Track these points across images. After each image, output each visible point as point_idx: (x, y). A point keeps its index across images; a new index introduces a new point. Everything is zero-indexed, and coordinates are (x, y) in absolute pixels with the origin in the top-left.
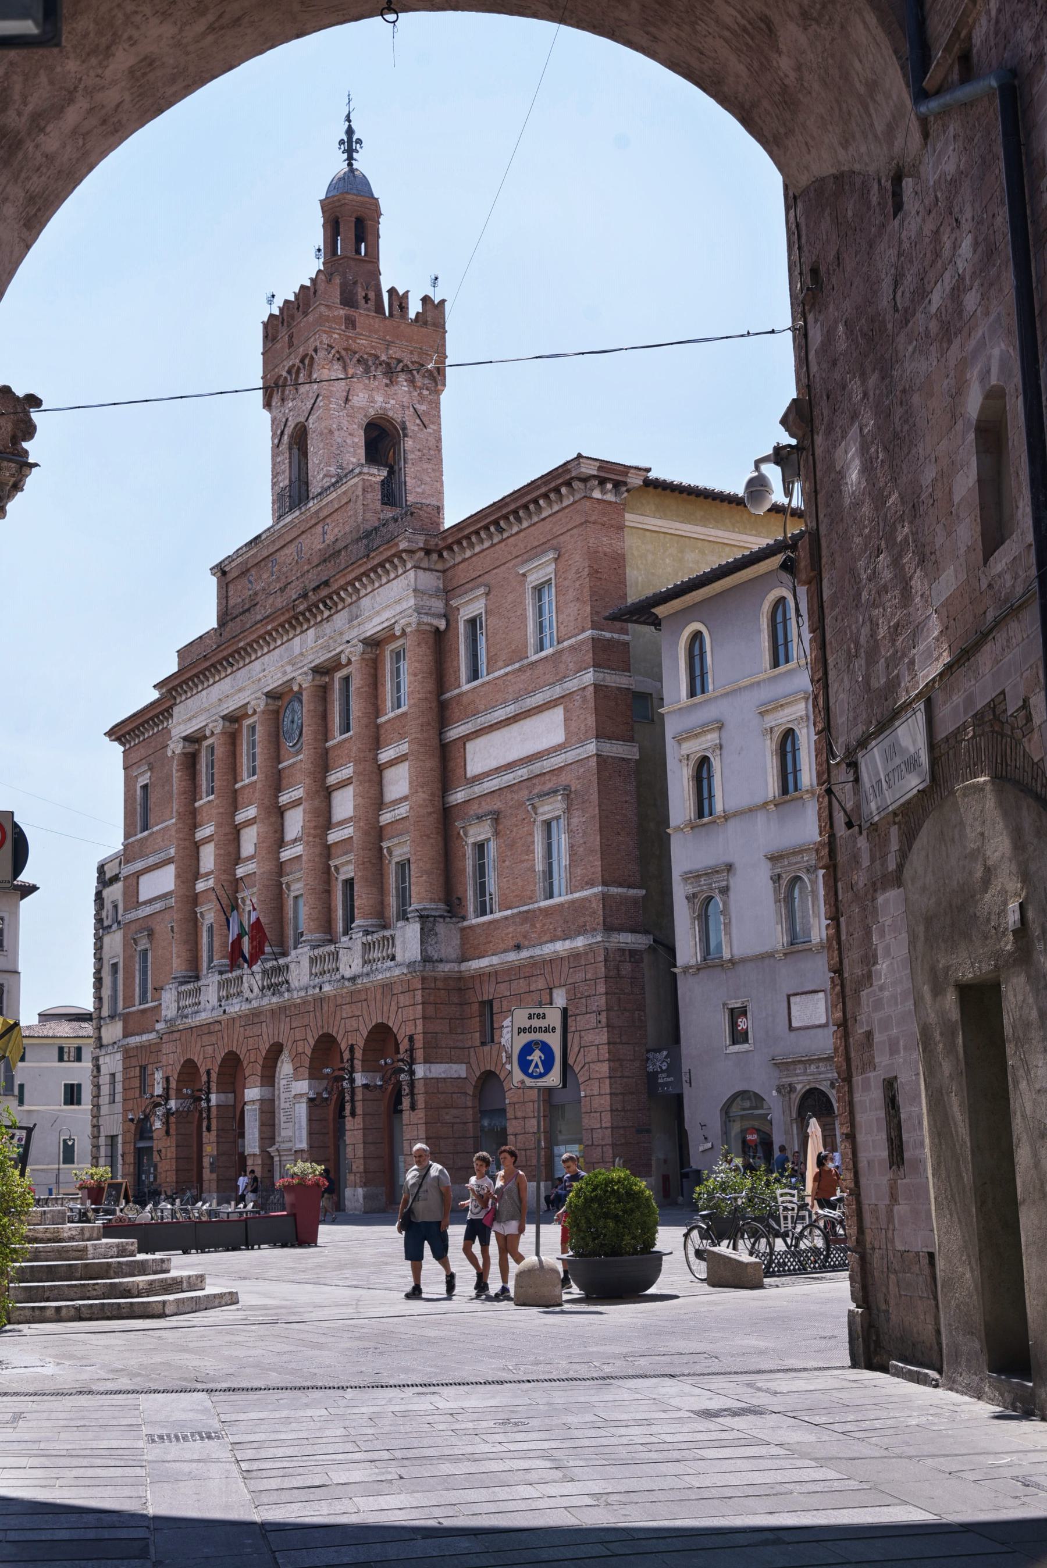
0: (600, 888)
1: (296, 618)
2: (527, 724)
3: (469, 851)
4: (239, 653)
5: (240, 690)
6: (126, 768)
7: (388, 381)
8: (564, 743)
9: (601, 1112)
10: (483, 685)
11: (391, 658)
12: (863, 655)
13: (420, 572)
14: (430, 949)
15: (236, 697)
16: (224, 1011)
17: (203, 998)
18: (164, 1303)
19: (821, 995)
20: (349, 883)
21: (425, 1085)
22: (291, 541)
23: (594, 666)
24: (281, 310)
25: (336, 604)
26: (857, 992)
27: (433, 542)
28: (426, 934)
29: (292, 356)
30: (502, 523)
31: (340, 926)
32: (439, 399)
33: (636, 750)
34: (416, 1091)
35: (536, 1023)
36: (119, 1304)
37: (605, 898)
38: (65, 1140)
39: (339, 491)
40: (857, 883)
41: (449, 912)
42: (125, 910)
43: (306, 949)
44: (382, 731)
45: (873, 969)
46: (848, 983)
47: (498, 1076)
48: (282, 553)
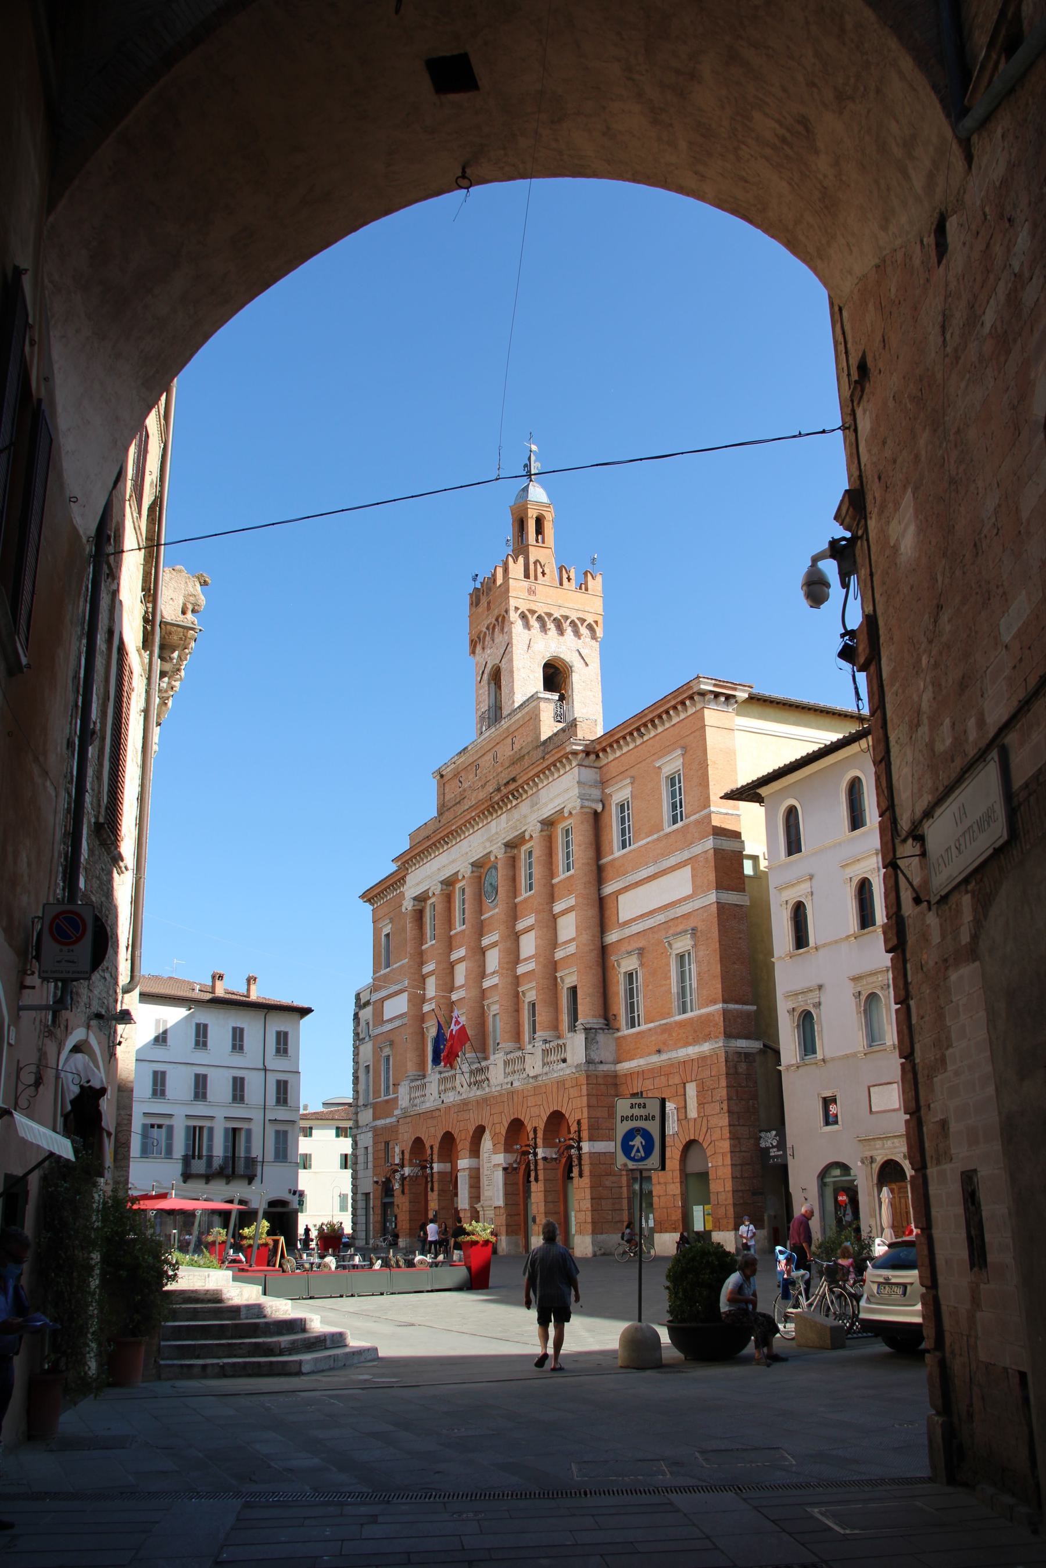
1: (491, 808)
5: (453, 861)
10: (630, 852)
12: (926, 721)
14: (592, 1053)
17: (427, 1092)
18: (300, 1362)
19: (895, 1085)
21: (590, 1157)
25: (521, 795)
26: (930, 1077)
28: (589, 1042)
30: (642, 730)
33: (747, 898)
35: (637, 1112)
36: (259, 1363)
37: (725, 1012)
40: (927, 963)
42: (374, 1026)
44: (556, 889)
45: (948, 1053)
46: (919, 1068)
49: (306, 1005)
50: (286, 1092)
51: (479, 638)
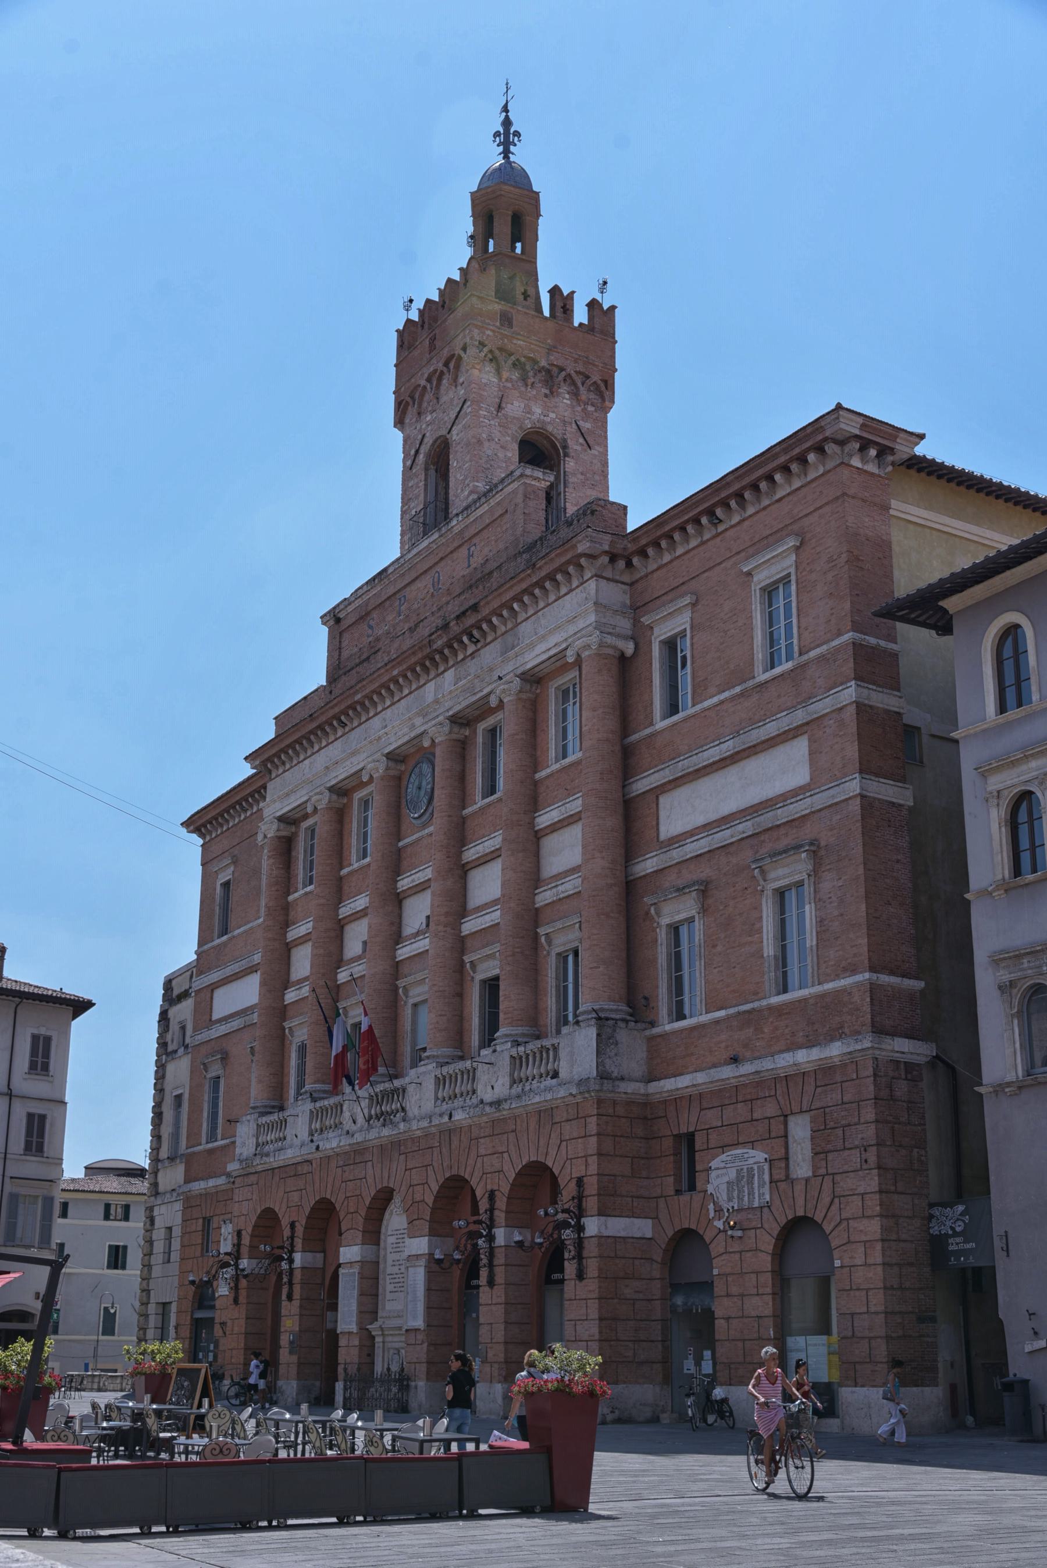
0: (867, 975)
1: (429, 660)
2: (752, 766)
3: (662, 935)
4: (355, 709)
5: (354, 754)
6: (204, 864)
7: (547, 392)
8: (809, 784)
9: (868, 1290)
10: (685, 720)
11: (556, 698)
13: (603, 583)
14: (608, 1062)
15: (348, 763)
16: (318, 1148)
17: (289, 1132)
20: (492, 985)
21: (600, 1245)
22: (426, 572)
23: (855, 679)
24: (421, 312)
27: (620, 545)
28: (604, 1042)
29: (434, 361)
30: (719, 512)
31: (475, 1038)
32: (606, 418)
33: (909, 793)
34: (585, 1254)
37: (873, 988)
38: (106, 1309)
39: (492, 502)
41: (631, 1015)
42: (195, 1030)
43: (430, 1067)
47: (701, 1237)
48: (413, 587)
49: (87, 996)
50: (41, 1134)
51: (412, 397)
